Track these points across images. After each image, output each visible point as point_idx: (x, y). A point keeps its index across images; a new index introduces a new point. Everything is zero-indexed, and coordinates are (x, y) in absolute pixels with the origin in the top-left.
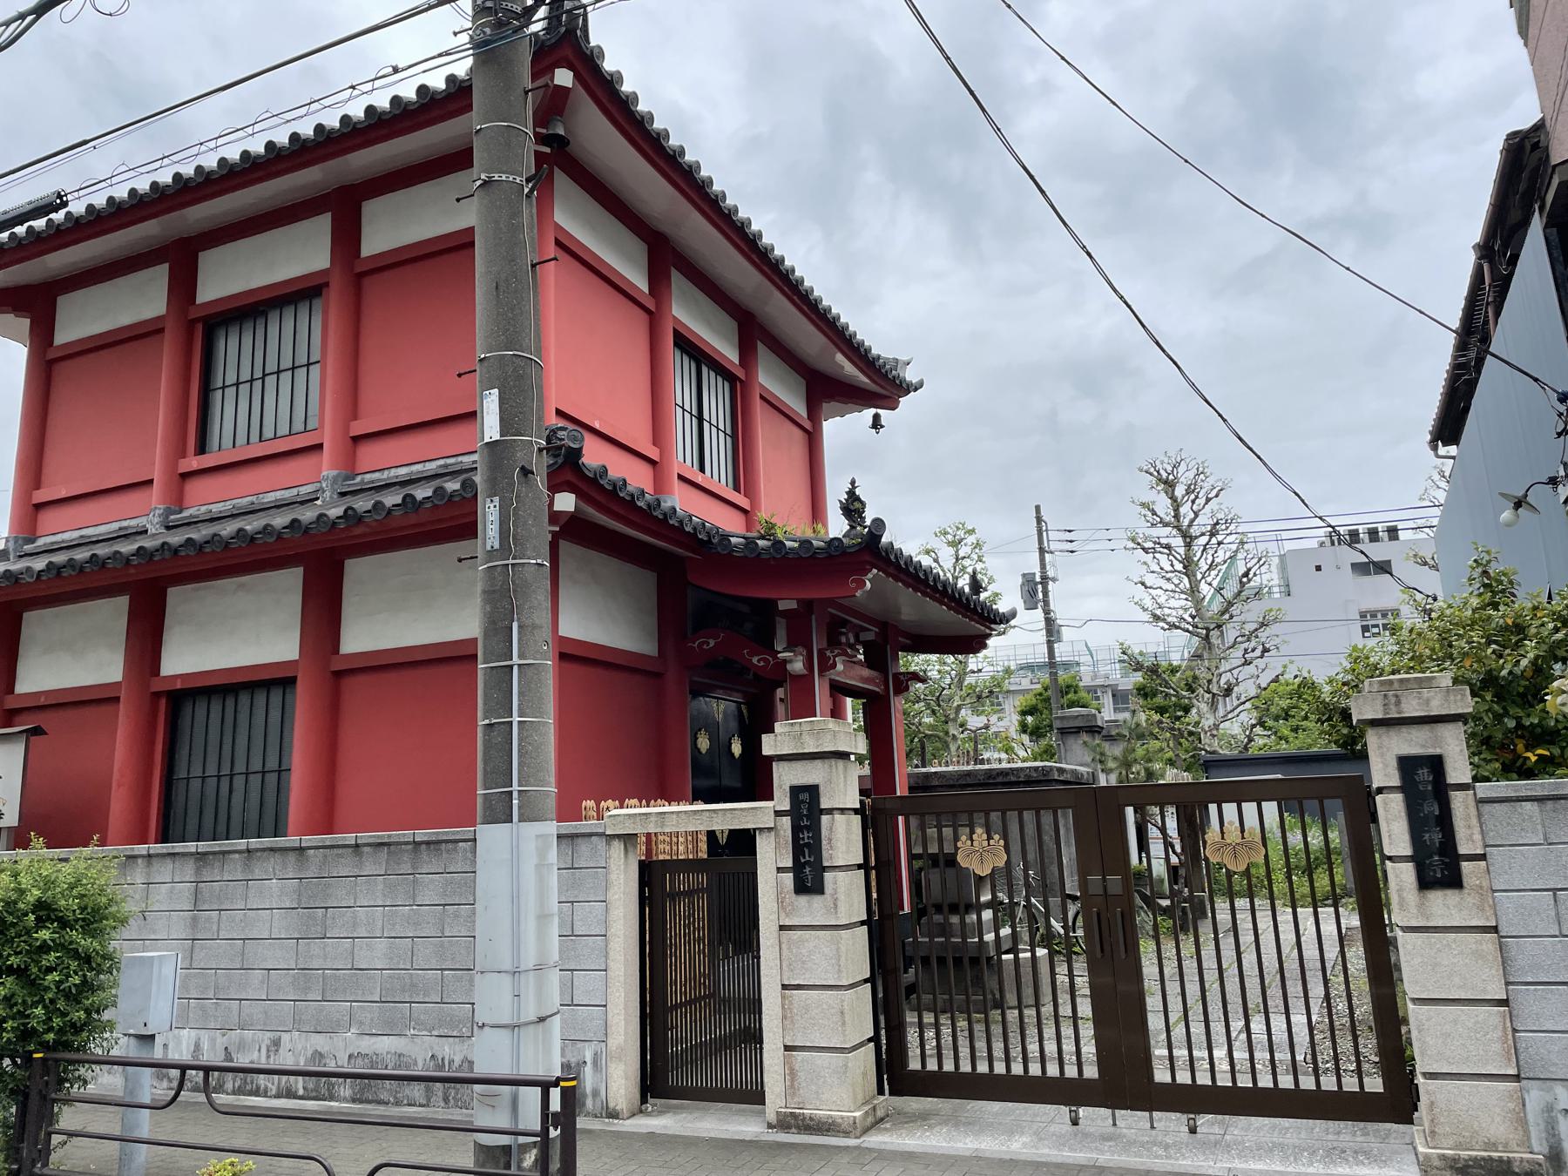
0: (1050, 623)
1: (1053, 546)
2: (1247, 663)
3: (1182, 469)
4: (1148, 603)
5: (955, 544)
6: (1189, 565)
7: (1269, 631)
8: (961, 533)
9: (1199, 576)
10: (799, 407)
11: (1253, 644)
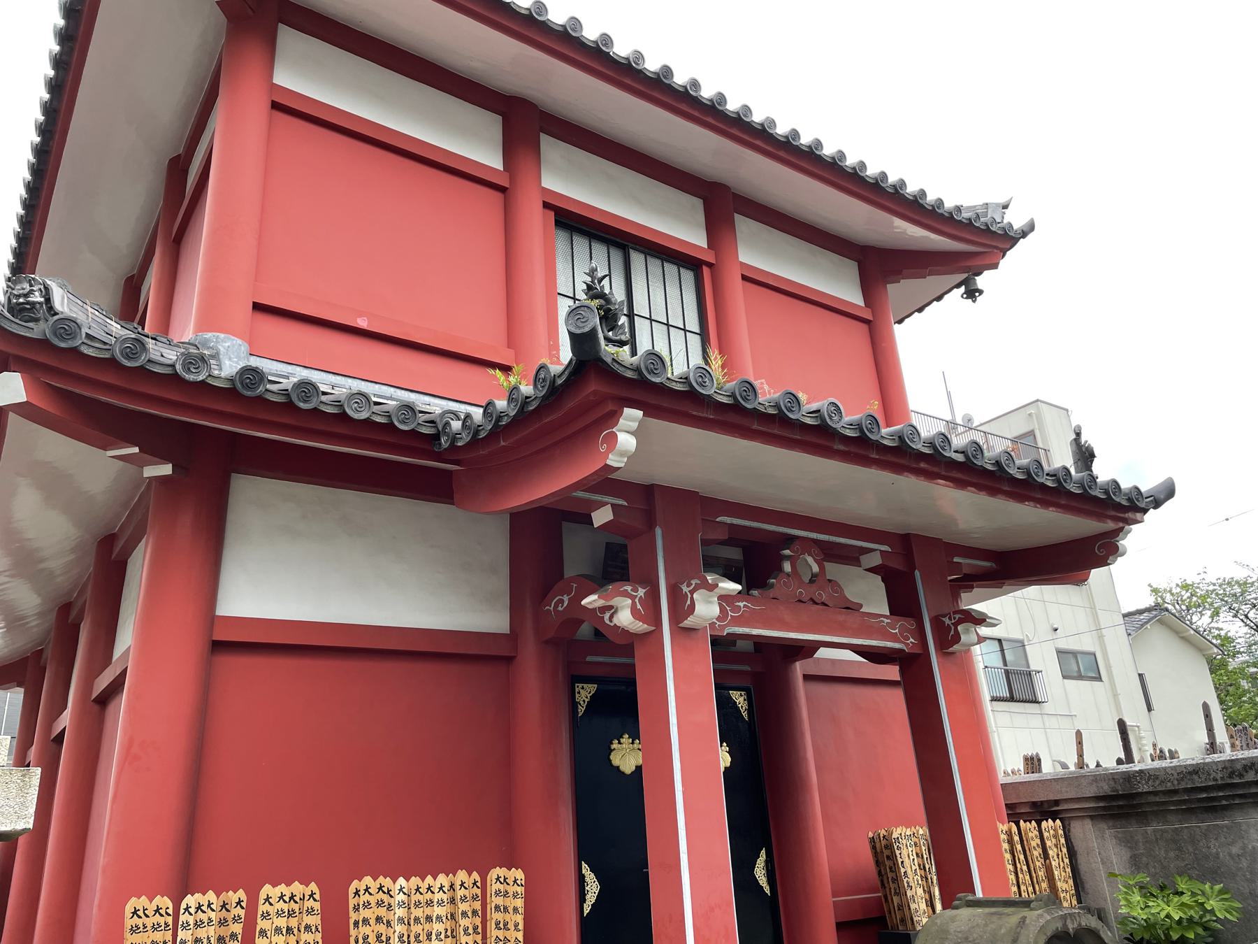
10: (852, 295)
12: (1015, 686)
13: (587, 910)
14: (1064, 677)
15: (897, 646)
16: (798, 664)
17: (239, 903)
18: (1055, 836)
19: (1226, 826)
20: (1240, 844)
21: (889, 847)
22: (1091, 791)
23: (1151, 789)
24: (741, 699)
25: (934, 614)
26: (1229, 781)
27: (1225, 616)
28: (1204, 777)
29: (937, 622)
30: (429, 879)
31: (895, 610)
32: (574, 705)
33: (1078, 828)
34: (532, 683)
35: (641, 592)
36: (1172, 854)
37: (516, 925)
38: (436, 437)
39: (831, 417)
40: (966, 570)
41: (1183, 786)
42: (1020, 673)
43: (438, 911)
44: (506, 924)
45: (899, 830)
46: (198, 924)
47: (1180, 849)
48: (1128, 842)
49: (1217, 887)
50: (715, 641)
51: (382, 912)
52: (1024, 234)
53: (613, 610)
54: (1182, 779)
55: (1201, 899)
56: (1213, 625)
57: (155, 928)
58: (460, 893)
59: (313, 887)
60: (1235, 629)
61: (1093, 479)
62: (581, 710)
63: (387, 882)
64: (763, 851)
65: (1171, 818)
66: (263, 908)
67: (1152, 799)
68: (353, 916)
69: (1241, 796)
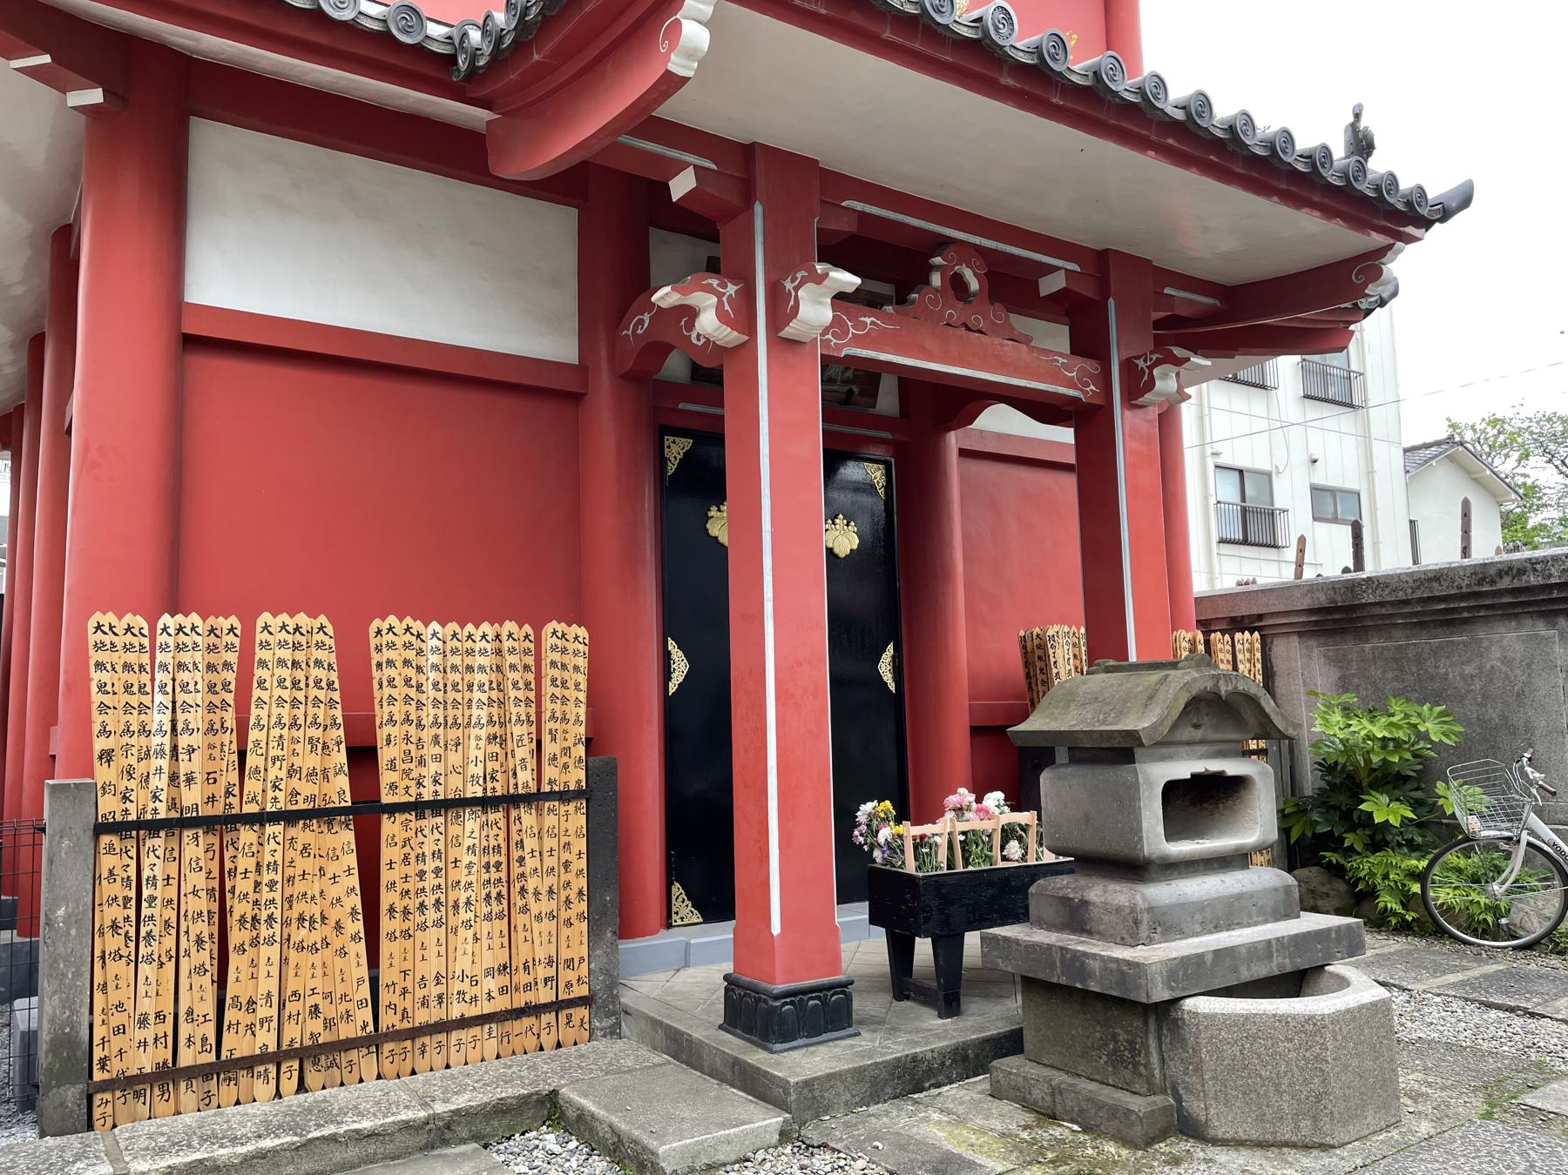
12: (1251, 527)
13: (672, 688)
14: (1315, 519)
15: (1072, 392)
16: (952, 433)
17: (232, 630)
18: (1250, 651)
20: (1476, 663)
21: (1042, 647)
24: (878, 474)
25: (1125, 356)
26: (1477, 589)
27: (1536, 460)
29: (1128, 366)
30: (470, 627)
31: (1077, 349)
32: (662, 461)
33: (1280, 648)
34: (607, 425)
35: (731, 289)
36: (1390, 675)
37: (577, 685)
38: (451, 60)
39: (997, 29)
40: (1181, 311)
41: (1418, 595)
42: (1259, 512)
43: (480, 660)
44: (564, 683)
45: (1056, 628)
46: (180, 648)
47: (1401, 669)
48: (1339, 661)
49: (1438, 709)
50: (827, 361)
51: (411, 655)
52: (1445, 214)
53: (691, 313)
55: (1414, 720)
56: (1520, 470)
57: (127, 648)
58: (508, 644)
59: (323, 619)
60: (1541, 473)
61: (1362, 169)
62: (671, 468)
63: (417, 626)
64: (891, 647)
65: (1397, 633)
66: (261, 637)
68: (375, 658)
69: (1488, 607)
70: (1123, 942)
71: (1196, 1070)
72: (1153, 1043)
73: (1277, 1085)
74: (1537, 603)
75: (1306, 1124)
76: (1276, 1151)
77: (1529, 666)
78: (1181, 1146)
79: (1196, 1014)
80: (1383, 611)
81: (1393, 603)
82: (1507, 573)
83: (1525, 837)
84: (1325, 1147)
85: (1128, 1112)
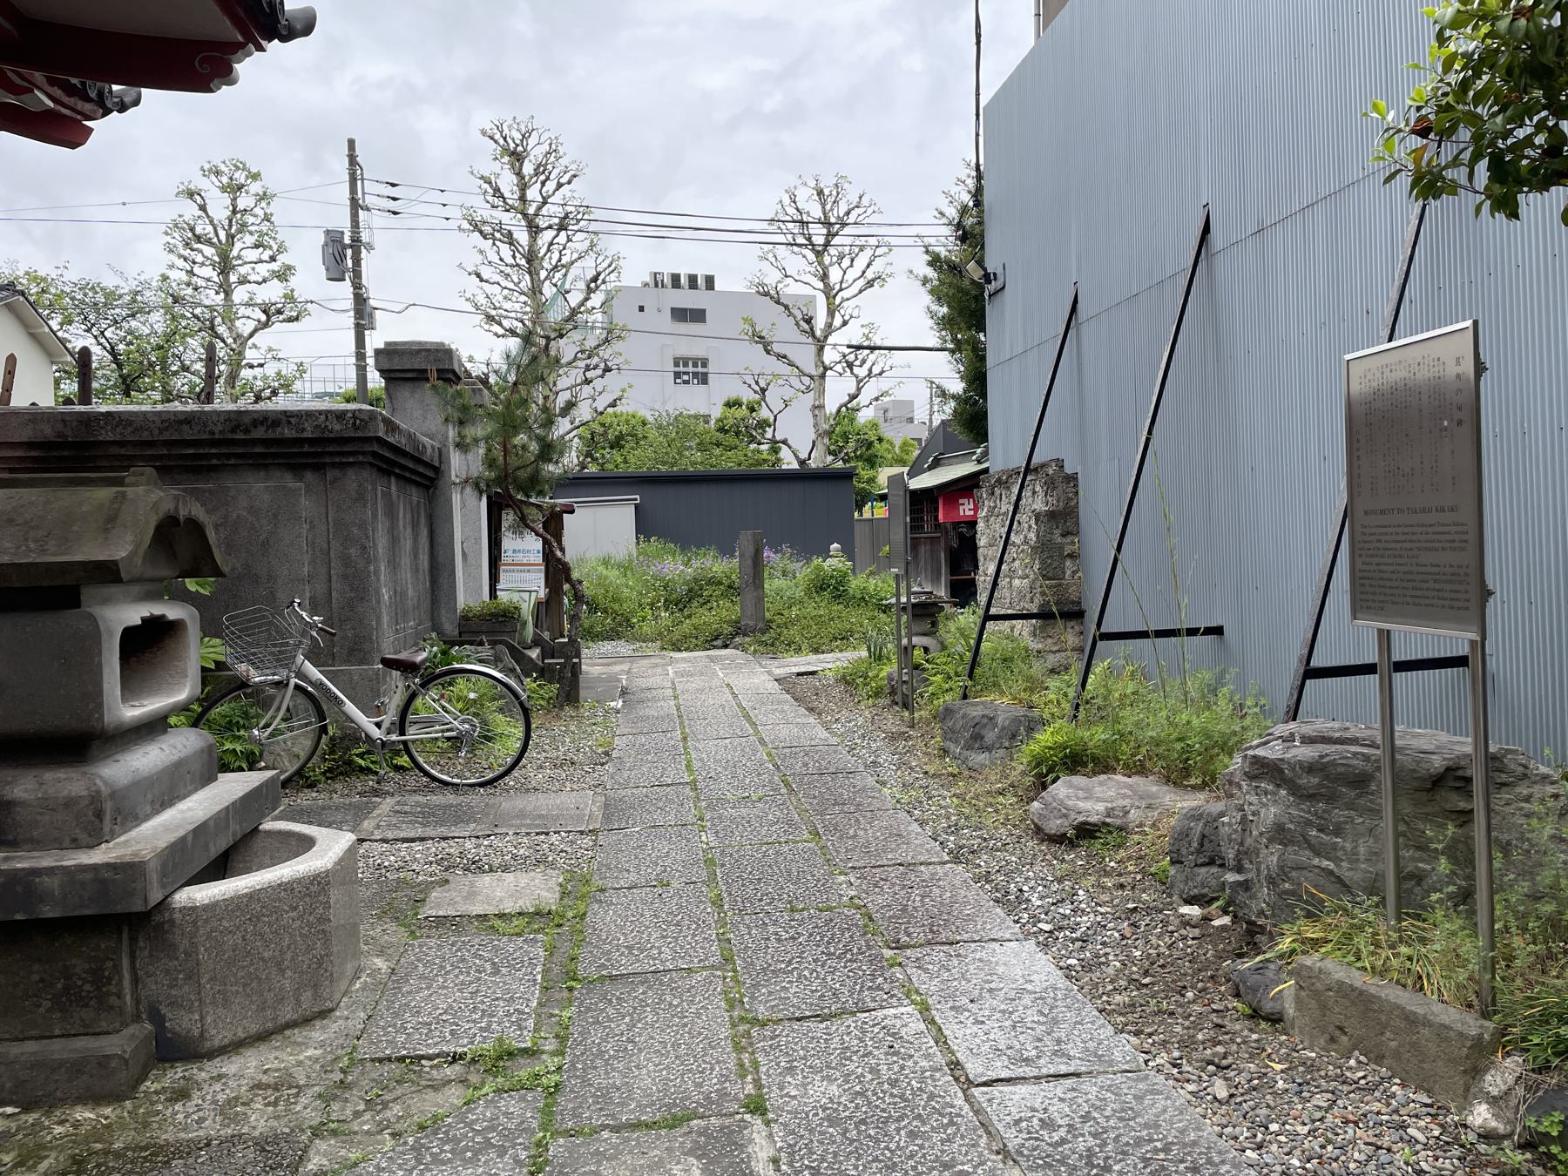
0: (360, 301)
1: (369, 200)
2: (588, 382)
3: (532, 141)
4: (481, 300)
5: (234, 189)
6: (532, 257)
7: (617, 346)
8: (240, 177)
9: (543, 274)
11: (595, 360)
19: (210, 491)
22: (24, 435)
23: (118, 438)
26: (230, 436)
28: (197, 428)
41: (166, 436)
54: (167, 429)
67: (115, 450)
70: (76, 845)
71: (189, 977)
72: (125, 962)
73: (279, 964)
74: (288, 455)
75: (307, 996)
76: (280, 1037)
77: (275, 516)
78: (175, 1074)
79: (194, 909)
80: (123, 451)
81: (135, 444)
82: (262, 423)
83: (294, 681)
84: (324, 1014)
85: (103, 1061)
